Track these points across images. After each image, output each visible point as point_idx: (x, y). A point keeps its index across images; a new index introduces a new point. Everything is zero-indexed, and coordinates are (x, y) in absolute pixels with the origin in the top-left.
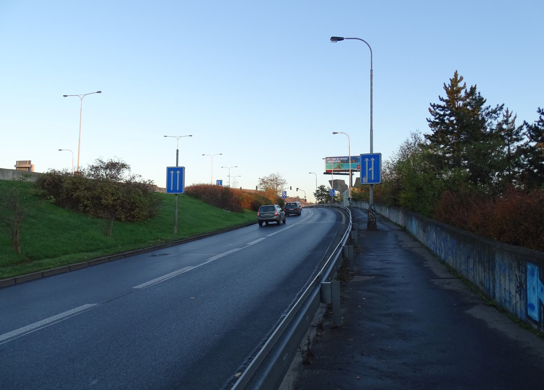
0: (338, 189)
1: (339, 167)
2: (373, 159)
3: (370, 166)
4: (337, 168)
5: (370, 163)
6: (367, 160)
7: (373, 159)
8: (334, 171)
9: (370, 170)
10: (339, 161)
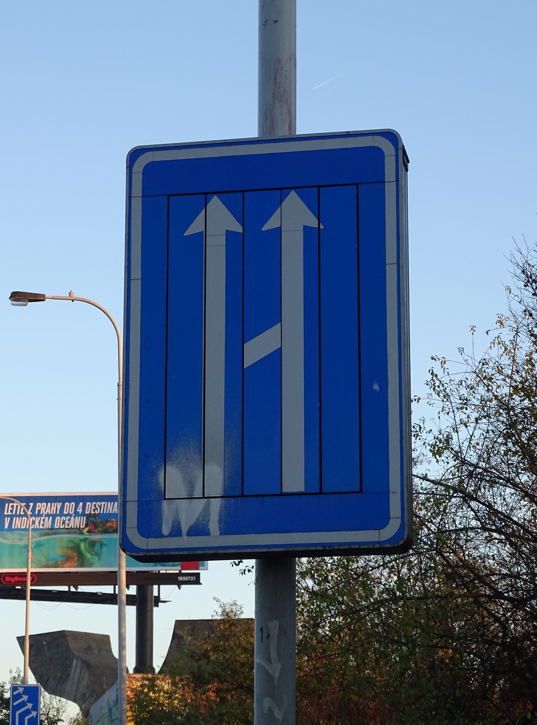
0: (68, 687)
1: (76, 554)
2: (293, 217)
3: (252, 309)
4: (68, 559)
5: (253, 257)
6: (217, 221)
7: (293, 217)
8: (38, 578)
9: (255, 350)
10: (78, 522)
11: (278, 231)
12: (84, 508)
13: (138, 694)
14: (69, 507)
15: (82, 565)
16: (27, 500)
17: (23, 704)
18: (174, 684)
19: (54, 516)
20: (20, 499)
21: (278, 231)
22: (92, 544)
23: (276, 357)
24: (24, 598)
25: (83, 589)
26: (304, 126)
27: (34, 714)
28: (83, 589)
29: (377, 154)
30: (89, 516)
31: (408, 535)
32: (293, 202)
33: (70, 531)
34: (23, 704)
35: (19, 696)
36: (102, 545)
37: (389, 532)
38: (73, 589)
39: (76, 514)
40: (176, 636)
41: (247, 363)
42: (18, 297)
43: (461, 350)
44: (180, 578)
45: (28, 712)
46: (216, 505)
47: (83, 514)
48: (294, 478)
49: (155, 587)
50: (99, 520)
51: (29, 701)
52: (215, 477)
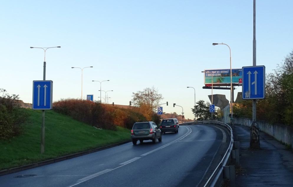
1: (219, 80)
2: (256, 73)
3: (252, 80)
4: (218, 82)
7: (256, 73)
8: (214, 85)
9: (253, 83)
10: (220, 75)
11: (254, 74)
12: (221, 72)
13: (233, 106)
14: (218, 72)
15: (221, 83)
16: (210, 71)
17: (212, 108)
18: (239, 105)
19: (215, 74)
20: (209, 71)
21: (254, 74)
22: (222, 79)
23: (254, 84)
24: (211, 89)
25: (221, 87)
26: (257, 65)
27: (214, 110)
28: (221, 87)
29: (263, 67)
30: (222, 73)
31: (236, 127)
32: (256, 71)
33: (218, 76)
34: (212, 108)
35: (211, 107)
36: (224, 79)
37: (263, 98)
38: (219, 87)
39: (219, 73)
40: (238, 95)
41: (252, 84)
42: (214, 44)
43: (281, 63)
44: (239, 85)
45: (212, 109)
46: (250, 96)
47: (220, 73)
48: (256, 94)
49: (234, 86)
50: (223, 74)
51: (213, 107)
52: (250, 93)
